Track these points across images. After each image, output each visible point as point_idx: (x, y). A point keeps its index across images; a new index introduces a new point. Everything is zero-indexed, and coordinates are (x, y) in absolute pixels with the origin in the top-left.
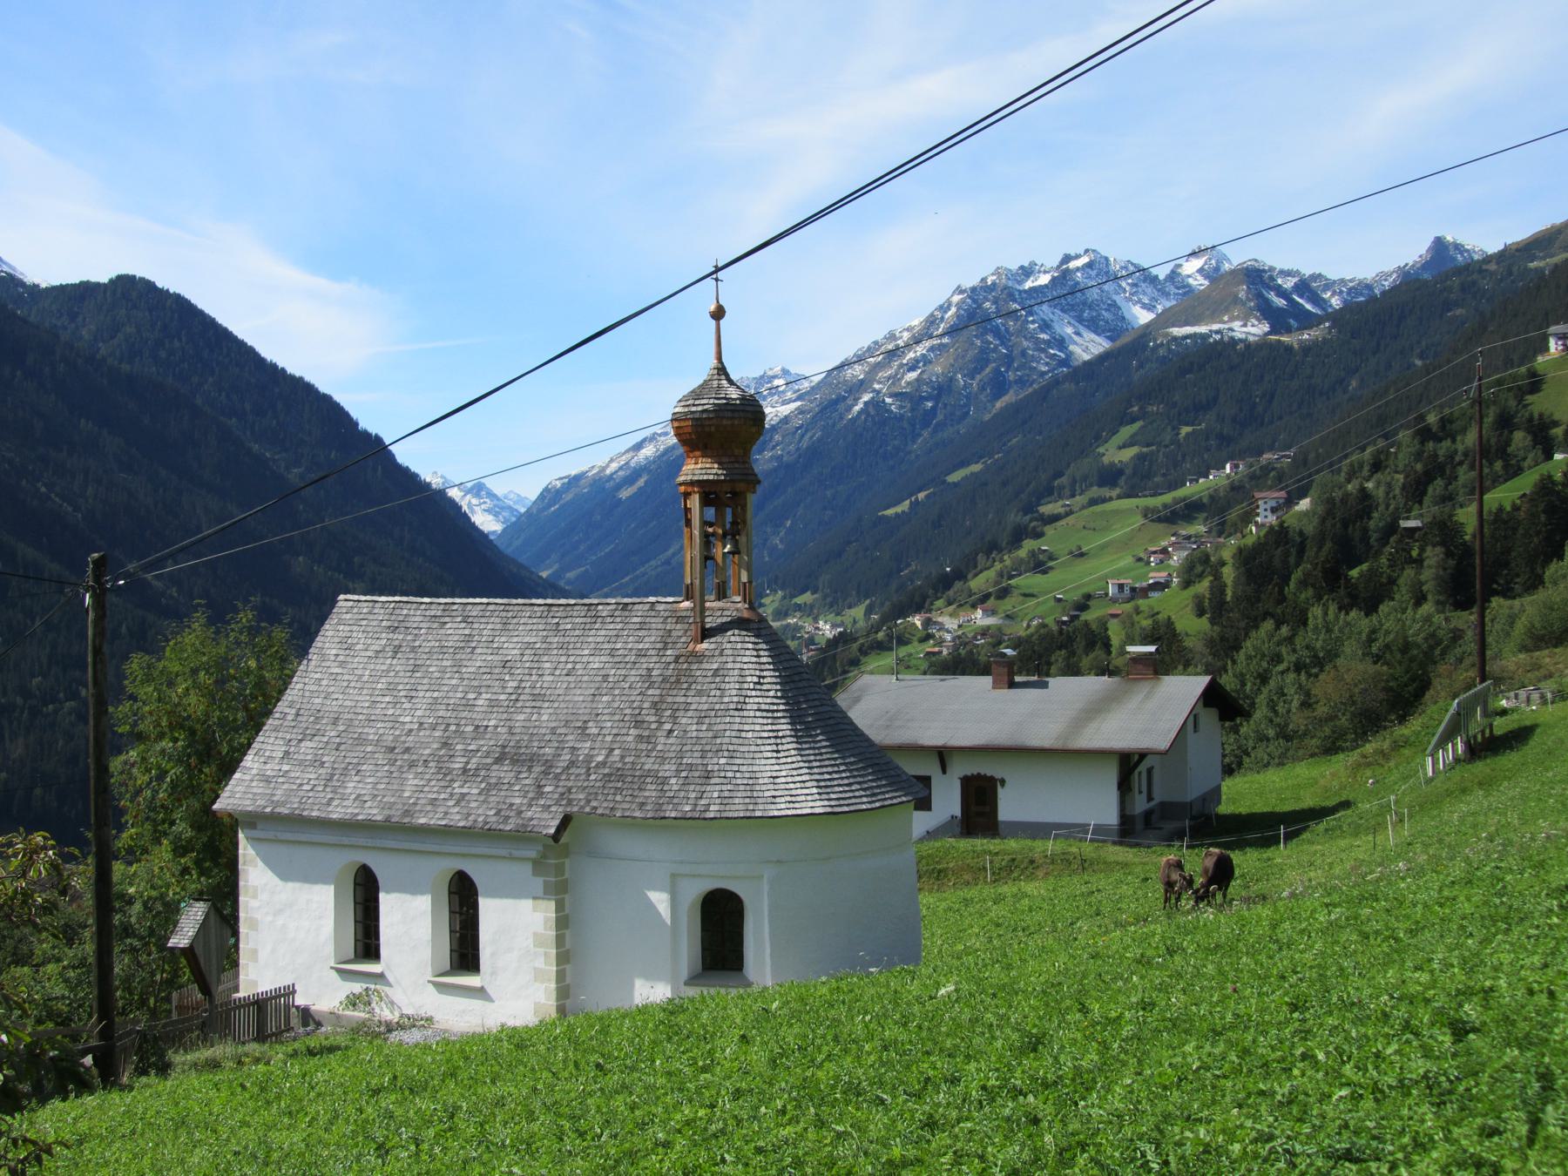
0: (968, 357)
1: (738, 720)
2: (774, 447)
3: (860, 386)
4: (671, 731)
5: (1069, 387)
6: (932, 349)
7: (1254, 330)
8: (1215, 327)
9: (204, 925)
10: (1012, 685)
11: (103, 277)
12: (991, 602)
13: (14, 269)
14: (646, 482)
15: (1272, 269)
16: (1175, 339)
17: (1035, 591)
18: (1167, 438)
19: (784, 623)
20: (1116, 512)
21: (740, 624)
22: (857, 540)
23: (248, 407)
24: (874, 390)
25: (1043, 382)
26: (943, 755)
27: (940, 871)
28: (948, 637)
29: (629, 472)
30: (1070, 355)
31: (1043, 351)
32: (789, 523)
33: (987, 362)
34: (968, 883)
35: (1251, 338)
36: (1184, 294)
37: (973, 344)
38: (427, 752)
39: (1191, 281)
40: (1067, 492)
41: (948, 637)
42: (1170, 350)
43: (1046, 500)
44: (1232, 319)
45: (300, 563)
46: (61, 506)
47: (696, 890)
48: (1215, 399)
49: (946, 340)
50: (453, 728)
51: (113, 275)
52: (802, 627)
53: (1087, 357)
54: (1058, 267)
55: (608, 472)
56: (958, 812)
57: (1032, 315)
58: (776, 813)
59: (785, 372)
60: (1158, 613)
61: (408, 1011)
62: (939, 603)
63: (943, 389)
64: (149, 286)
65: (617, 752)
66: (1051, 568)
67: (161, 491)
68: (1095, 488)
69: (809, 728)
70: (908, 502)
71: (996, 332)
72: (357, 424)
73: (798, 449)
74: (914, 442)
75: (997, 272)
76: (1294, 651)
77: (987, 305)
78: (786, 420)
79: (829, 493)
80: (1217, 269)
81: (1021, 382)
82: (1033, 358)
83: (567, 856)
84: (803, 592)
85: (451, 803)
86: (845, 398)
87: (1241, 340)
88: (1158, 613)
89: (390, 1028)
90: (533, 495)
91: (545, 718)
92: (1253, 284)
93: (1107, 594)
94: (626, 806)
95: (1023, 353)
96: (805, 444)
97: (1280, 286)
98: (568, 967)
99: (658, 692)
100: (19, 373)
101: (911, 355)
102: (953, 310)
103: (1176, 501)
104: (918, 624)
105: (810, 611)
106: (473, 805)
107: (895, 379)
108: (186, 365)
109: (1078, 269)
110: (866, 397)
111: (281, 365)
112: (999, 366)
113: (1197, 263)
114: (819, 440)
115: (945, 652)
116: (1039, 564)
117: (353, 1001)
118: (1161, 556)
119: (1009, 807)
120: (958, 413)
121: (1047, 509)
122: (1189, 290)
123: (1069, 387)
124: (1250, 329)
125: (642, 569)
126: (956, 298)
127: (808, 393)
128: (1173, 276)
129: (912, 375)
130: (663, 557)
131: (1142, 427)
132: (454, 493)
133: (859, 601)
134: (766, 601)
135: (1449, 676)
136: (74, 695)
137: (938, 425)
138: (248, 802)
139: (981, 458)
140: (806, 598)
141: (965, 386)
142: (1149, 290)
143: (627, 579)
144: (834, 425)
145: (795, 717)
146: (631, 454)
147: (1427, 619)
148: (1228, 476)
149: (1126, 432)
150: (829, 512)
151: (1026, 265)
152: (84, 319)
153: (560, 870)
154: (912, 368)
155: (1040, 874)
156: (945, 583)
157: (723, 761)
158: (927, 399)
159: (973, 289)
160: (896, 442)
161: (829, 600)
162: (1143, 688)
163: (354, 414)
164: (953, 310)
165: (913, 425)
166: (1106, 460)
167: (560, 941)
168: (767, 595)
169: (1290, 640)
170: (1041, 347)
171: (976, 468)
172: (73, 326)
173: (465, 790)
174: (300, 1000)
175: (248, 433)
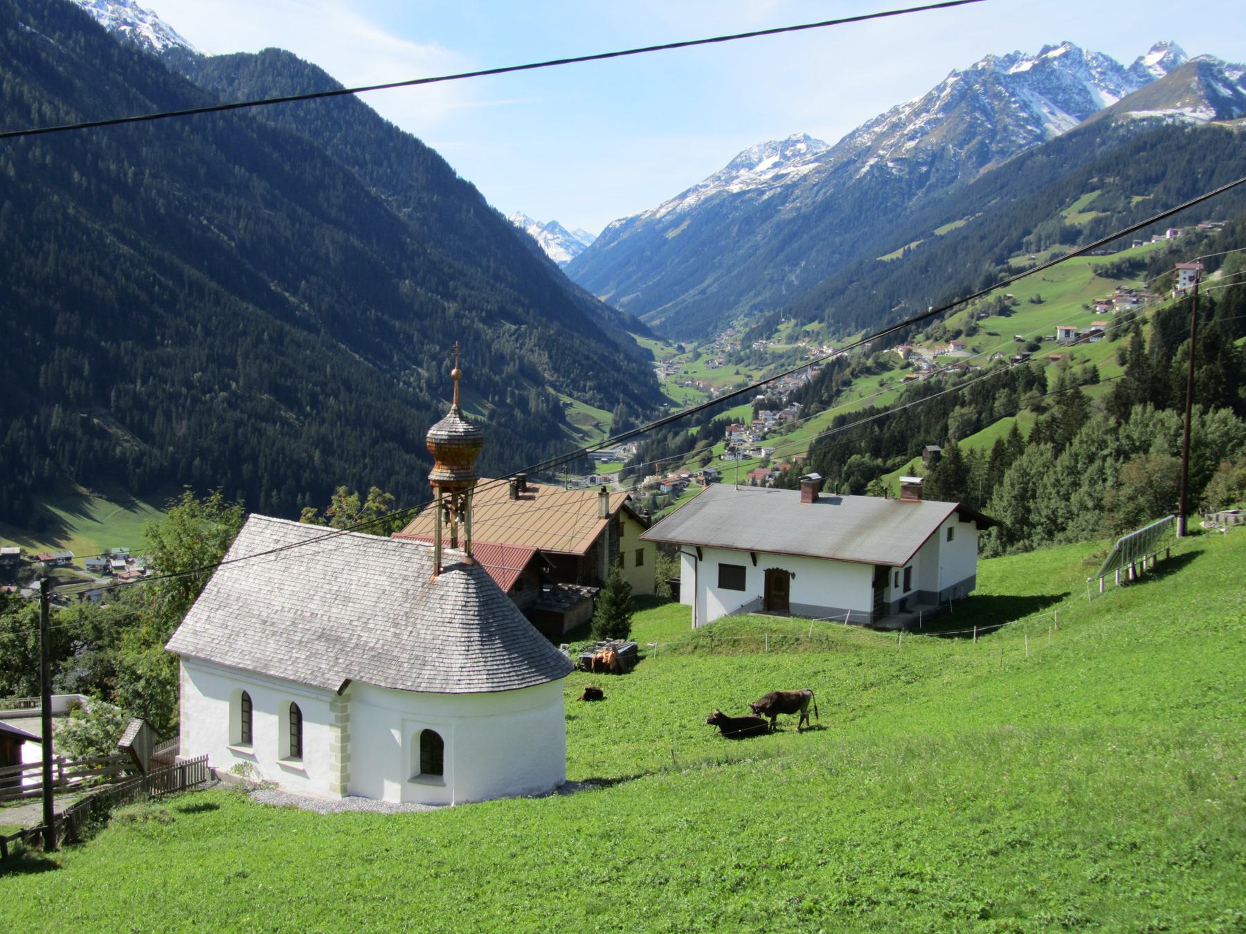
0: (959, 131)
1: (448, 629)
2: (794, 200)
3: (868, 151)
4: (411, 632)
5: (1040, 158)
6: (928, 122)
7: (1200, 115)
8: (1169, 112)
9: (140, 732)
10: (816, 500)
11: (254, 49)
12: (962, 338)
13: (185, 42)
14: (688, 226)
15: (1221, 63)
16: (1134, 121)
17: (998, 331)
18: (1120, 205)
19: (795, 346)
20: (1073, 267)
21: (460, 566)
22: (858, 280)
23: (368, 157)
24: (879, 156)
25: (1020, 153)
26: (754, 555)
27: (735, 641)
28: (925, 366)
29: (675, 216)
30: (1044, 131)
31: (1022, 127)
32: (803, 264)
33: (974, 135)
34: (752, 651)
35: (1199, 123)
36: (1145, 82)
37: (962, 119)
38: (283, 627)
39: (1151, 71)
40: (1033, 247)
41: (925, 366)
42: (1129, 131)
43: (1016, 253)
44: (1184, 105)
45: (406, 285)
46: (219, 236)
47: (416, 729)
48: (1164, 174)
49: (940, 115)
50: (299, 612)
51: (263, 48)
52: (809, 350)
53: (1059, 133)
54: (1039, 56)
55: (658, 216)
56: (762, 595)
57: (1014, 96)
58: (458, 691)
59: (806, 138)
60: (1088, 361)
61: (266, 778)
62: (920, 337)
63: (935, 157)
64: (292, 58)
65: (381, 642)
66: (1014, 312)
67: (297, 225)
68: (1057, 245)
69: (491, 635)
70: (901, 250)
71: (984, 111)
72: (454, 174)
73: (814, 203)
74: (910, 199)
75: (986, 59)
76: (1117, 439)
77: (977, 87)
78: (804, 178)
79: (837, 240)
80: (1174, 61)
81: (1002, 153)
82: (1013, 133)
83: (349, 701)
84: (811, 321)
85: (289, 663)
86: (855, 161)
87: (1190, 124)
88: (1088, 361)
89: (256, 788)
90: (597, 231)
91: (348, 613)
92: (1204, 76)
93: (1055, 338)
94: (378, 678)
95: (1005, 128)
96: (820, 198)
97: (1227, 79)
98: (349, 764)
99: (409, 605)
100: (187, 128)
101: (911, 127)
102: (948, 90)
103: (1123, 261)
104: (901, 354)
105: (815, 336)
106: (301, 665)
107: (897, 146)
108: (319, 122)
109: (1055, 59)
110: (872, 161)
111: (395, 124)
112: (984, 139)
113: (1158, 56)
114: (832, 195)
115: (921, 378)
116: (1005, 311)
117: (239, 769)
118: (1106, 306)
119: (798, 593)
120: (948, 177)
121: (1016, 262)
122: (1149, 79)
123: (1040, 158)
124: (1198, 114)
125: (683, 297)
126: (951, 80)
127: (824, 156)
128: (1136, 66)
129: (911, 144)
130: (700, 287)
131: (1100, 195)
132: (532, 230)
133: (857, 330)
134: (780, 327)
135: (1227, 472)
136: (226, 388)
137: (931, 185)
138: (184, 647)
139: (964, 215)
140: (814, 326)
141: (955, 155)
142: (1115, 78)
143: (670, 304)
144: (844, 183)
145: (484, 628)
146: (678, 202)
147: (1224, 421)
148: (1168, 241)
149: (1086, 199)
150: (837, 256)
151: (1011, 53)
152: (240, 84)
153: (344, 709)
154: (912, 138)
155: (801, 649)
156: (925, 319)
157: (435, 655)
158: (922, 164)
159: (966, 73)
160: (895, 200)
161: (832, 329)
162: (908, 508)
163: (453, 165)
164: (948, 90)
165: (910, 186)
166: (1068, 222)
167: (343, 750)
168: (782, 323)
169: (1114, 431)
170: (1020, 123)
171: (960, 224)
172: (230, 89)
173: (298, 655)
174: (211, 764)
175: (368, 178)
